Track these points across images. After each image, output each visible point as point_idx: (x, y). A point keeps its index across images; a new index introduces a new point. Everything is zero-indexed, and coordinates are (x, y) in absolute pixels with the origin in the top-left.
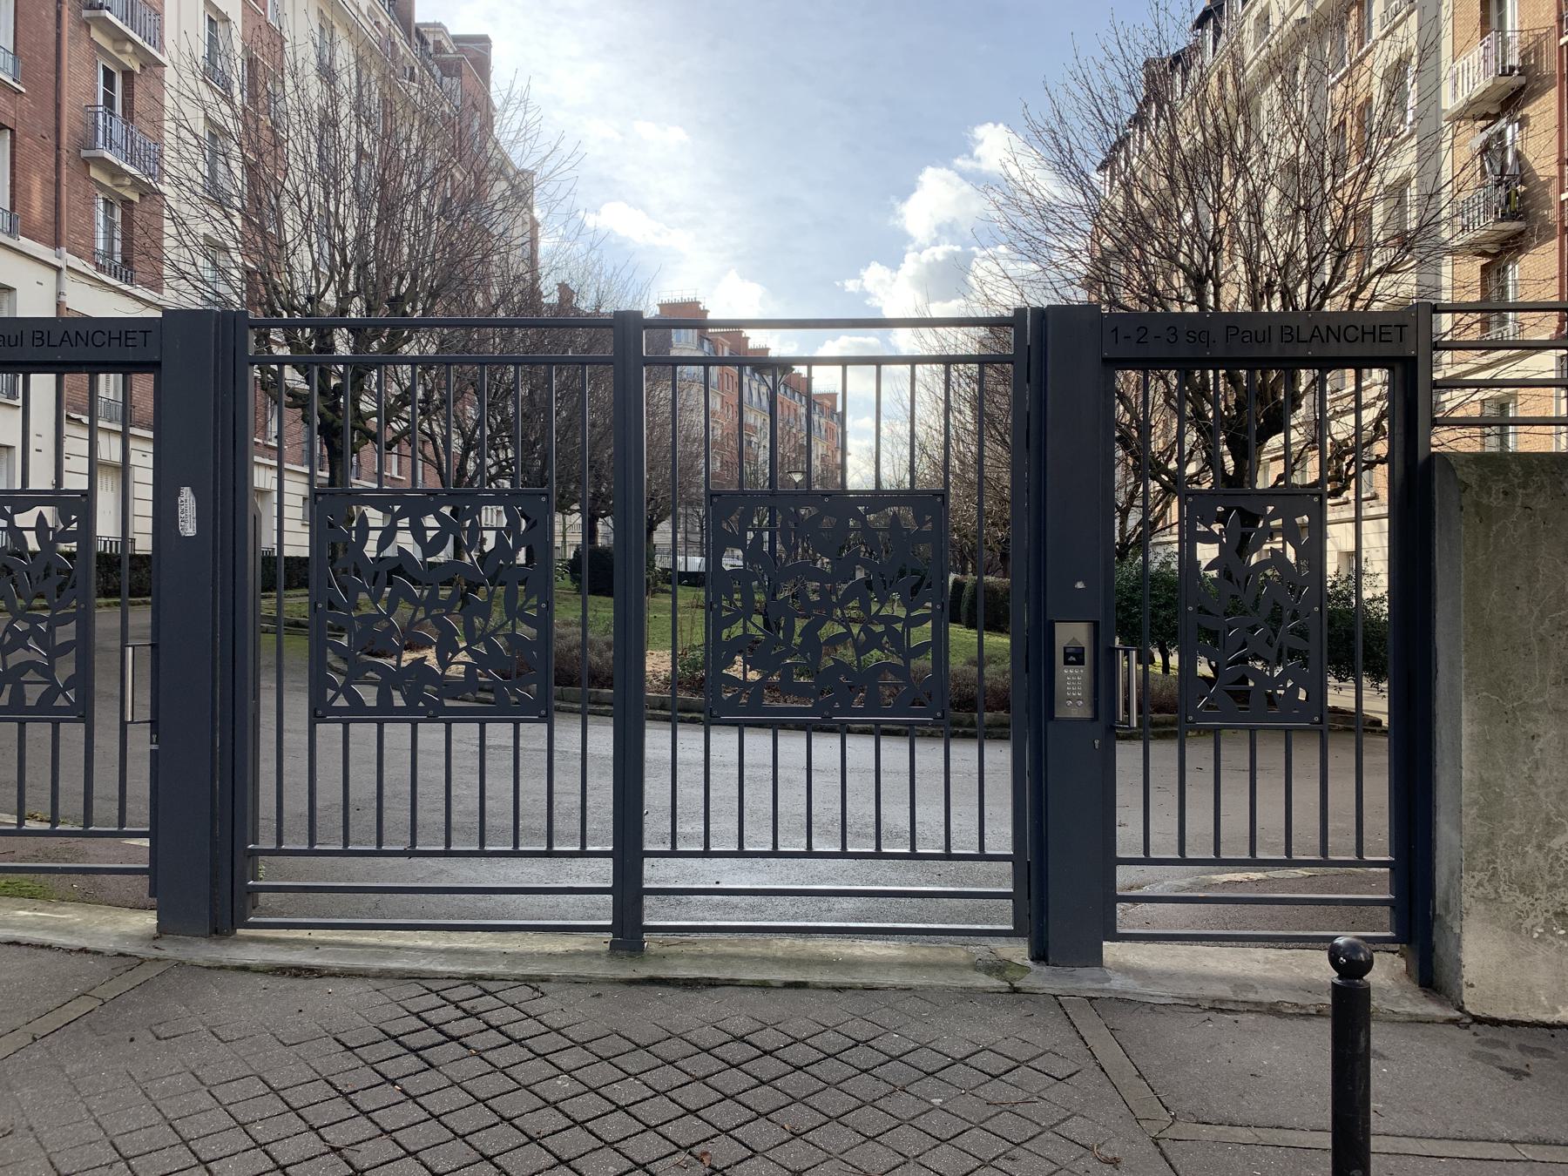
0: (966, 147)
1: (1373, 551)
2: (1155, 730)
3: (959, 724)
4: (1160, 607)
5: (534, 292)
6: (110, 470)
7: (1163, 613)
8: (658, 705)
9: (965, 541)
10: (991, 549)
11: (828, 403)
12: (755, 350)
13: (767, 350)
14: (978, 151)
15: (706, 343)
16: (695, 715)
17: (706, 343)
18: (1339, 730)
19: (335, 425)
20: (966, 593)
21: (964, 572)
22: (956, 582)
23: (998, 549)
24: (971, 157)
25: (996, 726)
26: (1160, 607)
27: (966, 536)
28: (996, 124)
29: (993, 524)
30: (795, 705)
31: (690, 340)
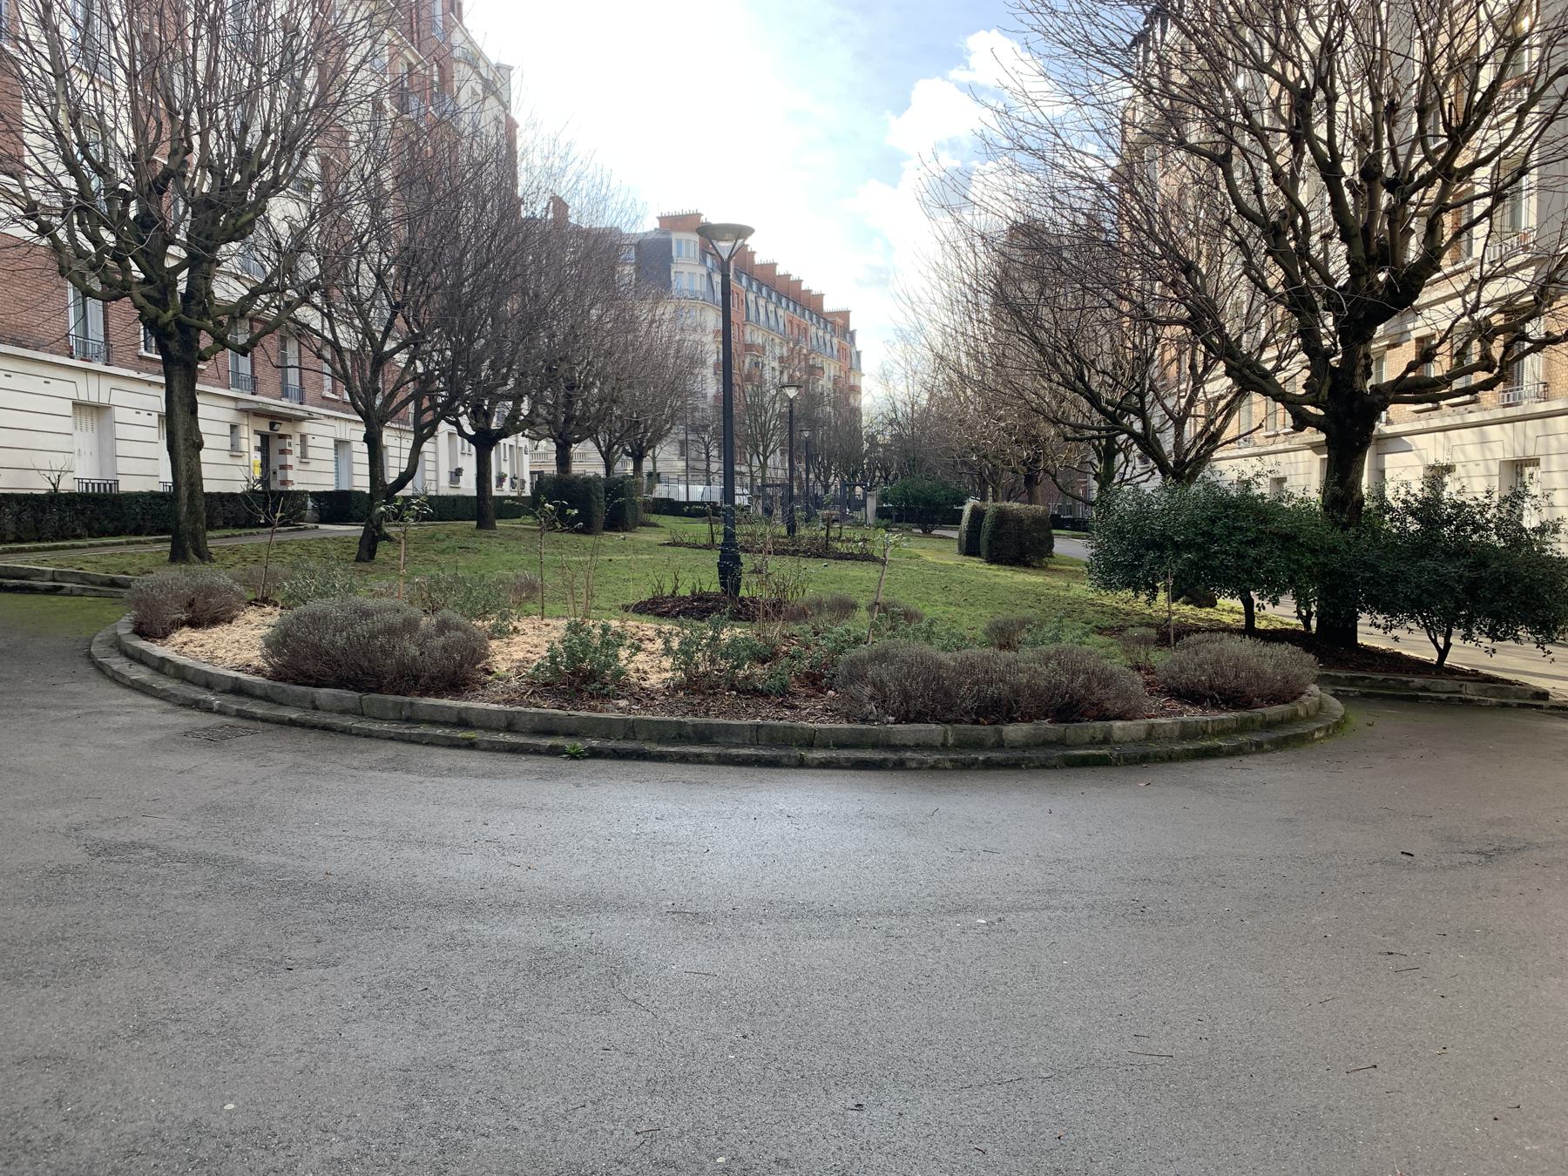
0: (959, 57)
1: (1471, 466)
2: (1273, 735)
3: (979, 745)
4: (1248, 543)
5: (512, 203)
6: (89, 410)
7: (1253, 552)
8: (503, 724)
9: (985, 462)
10: (1014, 471)
11: (839, 321)
12: (762, 266)
13: (773, 266)
14: (973, 61)
15: (709, 258)
16: (559, 741)
17: (709, 258)
18: (1492, 707)
19: (160, 322)
20: (987, 522)
21: (983, 499)
22: (975, 510)
23: (1022, 470)
24: (968, 69)
25: (1037, 745)
26: (1248, 543)
27: (985, 456)
28: (989, 31)
29: (1016, 441)
30: (721, 720)
31: (692, 255)
